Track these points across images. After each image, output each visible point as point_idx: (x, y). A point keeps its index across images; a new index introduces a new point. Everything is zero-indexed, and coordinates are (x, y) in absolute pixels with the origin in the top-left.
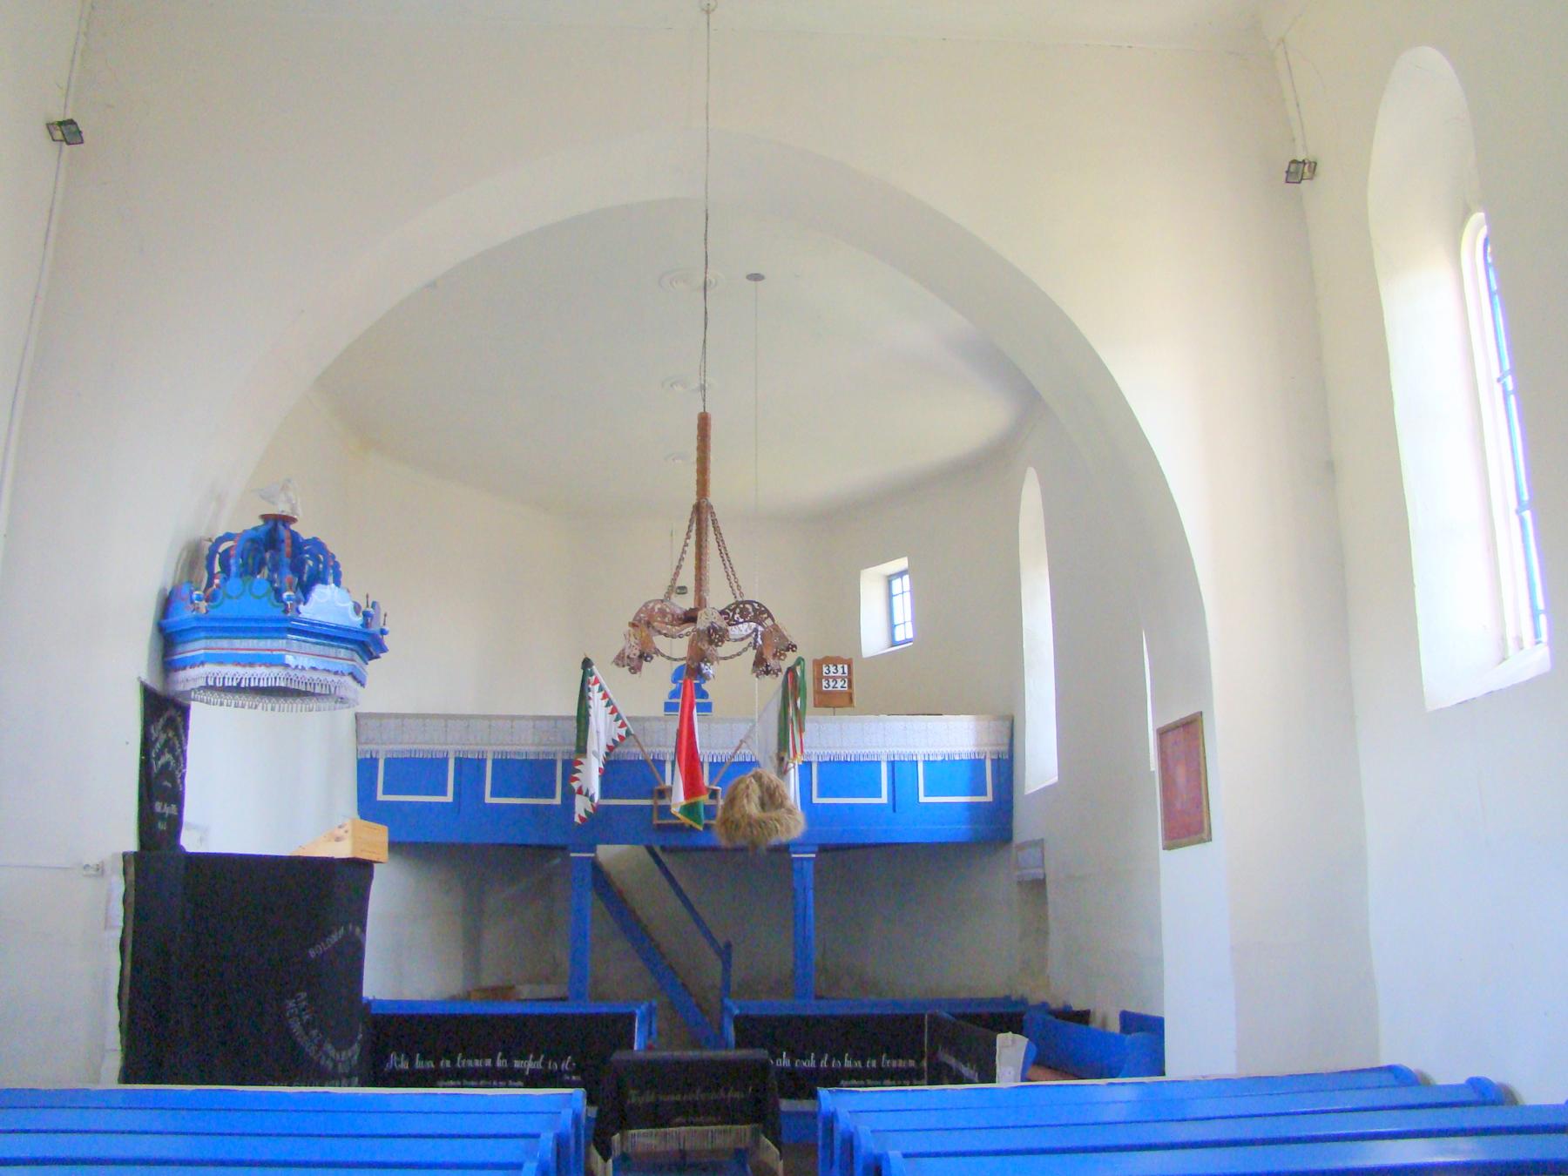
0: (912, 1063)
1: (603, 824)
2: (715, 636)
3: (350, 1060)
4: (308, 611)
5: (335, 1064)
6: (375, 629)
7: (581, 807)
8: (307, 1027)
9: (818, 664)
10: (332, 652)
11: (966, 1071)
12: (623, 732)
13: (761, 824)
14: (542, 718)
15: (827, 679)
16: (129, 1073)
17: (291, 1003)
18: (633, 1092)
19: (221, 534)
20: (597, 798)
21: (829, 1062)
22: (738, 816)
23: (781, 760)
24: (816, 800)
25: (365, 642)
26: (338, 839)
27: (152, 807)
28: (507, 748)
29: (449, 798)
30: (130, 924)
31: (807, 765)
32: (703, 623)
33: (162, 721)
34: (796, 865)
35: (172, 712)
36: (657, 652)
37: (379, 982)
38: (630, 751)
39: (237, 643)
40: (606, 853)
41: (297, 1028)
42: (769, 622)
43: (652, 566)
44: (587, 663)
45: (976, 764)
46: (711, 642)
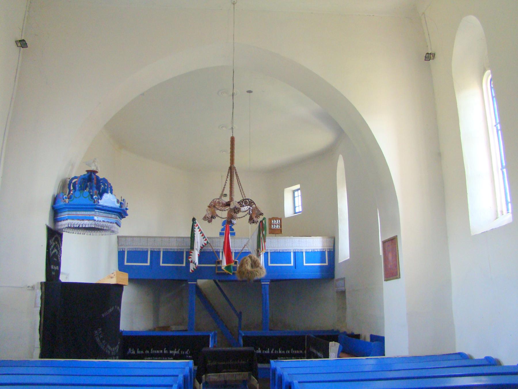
0: (301, 352)
1: (199, 272)
2: (236, 210)
3: (116, 350)
4: (102, 202)
5: (111, 352)
6: (124, 208)
7: (192, 267)
8: (101, 340)
9: (270, 220)
10: (110, 216)
11: (319, 354)
12: (206, 242)
13: (251, 272)
14: (179, 237)
15: (273, 225)
16: (43, 355)
17: (96, 332)
18: (209, 361)
19: (73, 177)
20: (197, 264)
21: (274, 351)
22: (244, 270)
23: (258, 251)
24: (270, 265)
25: (121, 212)
26: (112, 278)
27: (50, 267)
28: (167, 247)
29: (148, 264)
30: (43, 305)
31: (267, 253)
32: (232, 206)
33: (53, 239)
34: (263, 286)
35: (57, 236)
36: (217, 216)
37: (125, 325)
38: (208, 248)
39: (78, 213)
40: (200, 282)
41: (98, 340)
42: (254, 206)
43: (215, 187)
44: (194, 219)
45: (322, 253)
46: (235, 212)
